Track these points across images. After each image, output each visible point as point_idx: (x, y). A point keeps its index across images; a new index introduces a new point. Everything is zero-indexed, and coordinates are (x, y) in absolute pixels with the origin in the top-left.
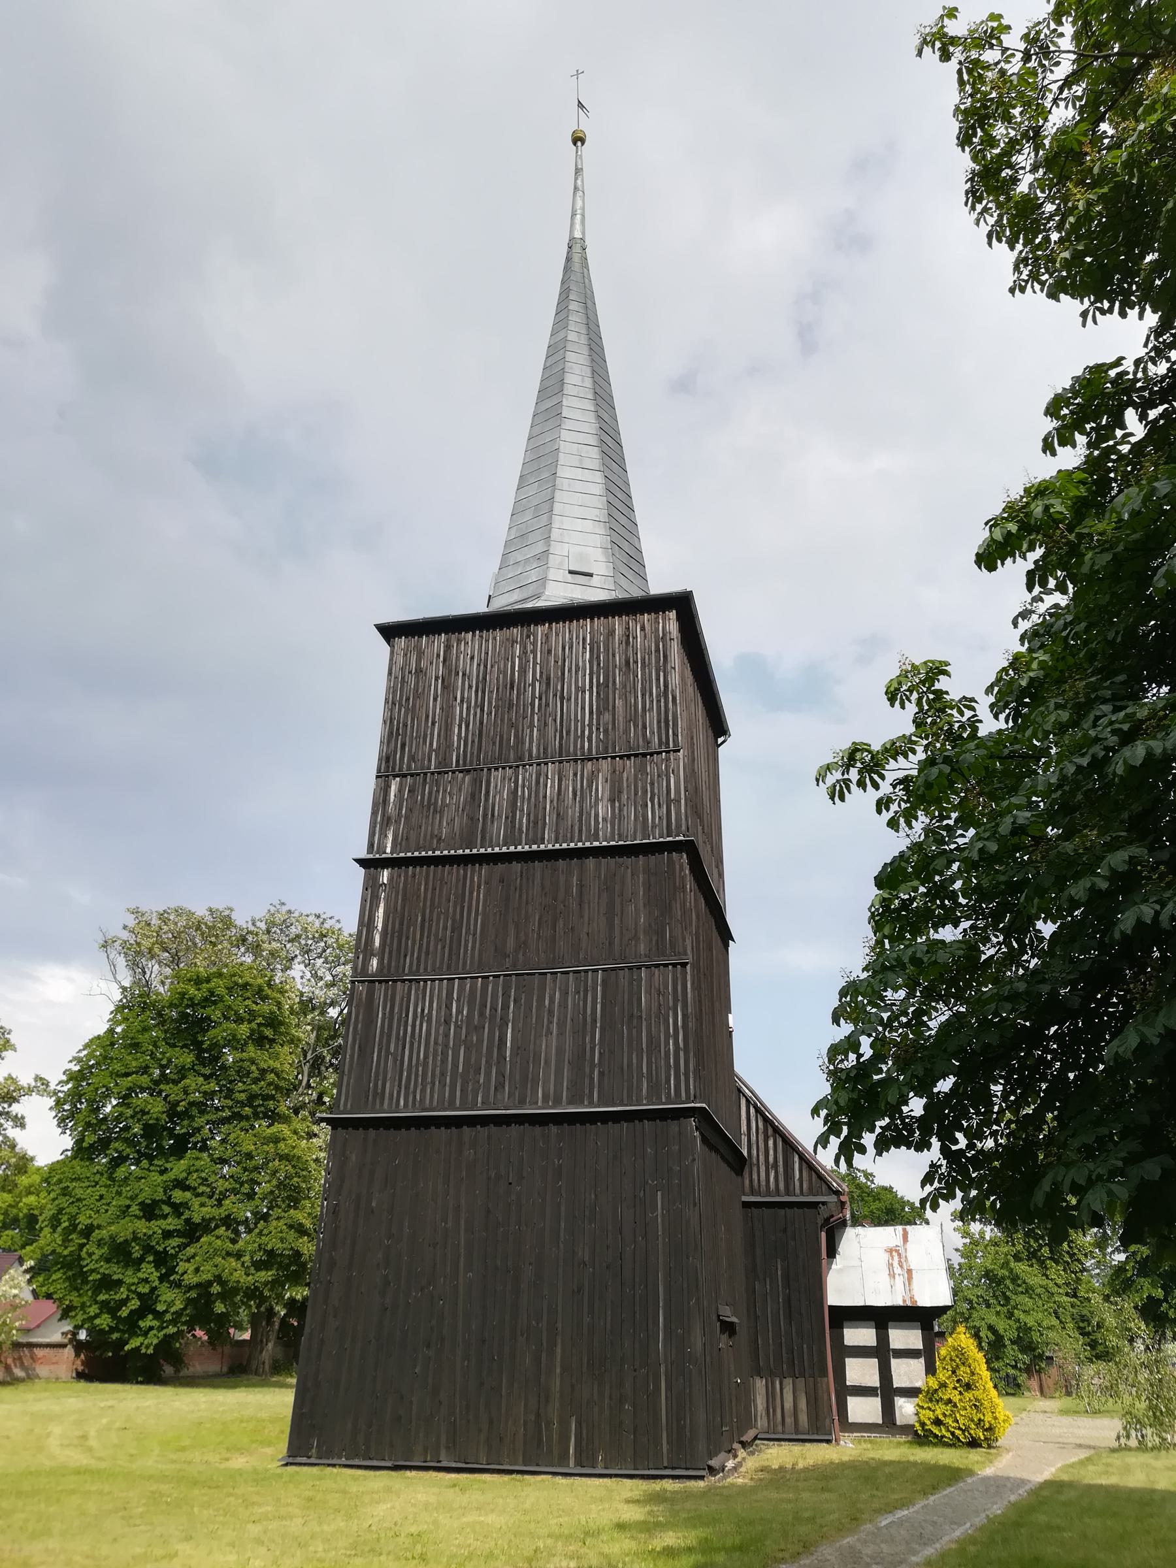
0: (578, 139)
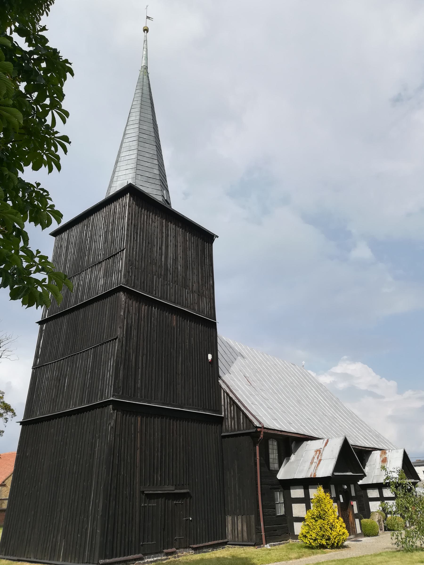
0: (146, 30)
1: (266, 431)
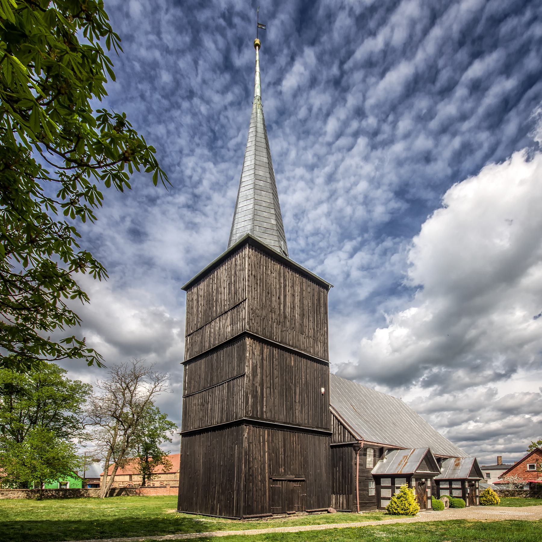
1: (366, 443)
